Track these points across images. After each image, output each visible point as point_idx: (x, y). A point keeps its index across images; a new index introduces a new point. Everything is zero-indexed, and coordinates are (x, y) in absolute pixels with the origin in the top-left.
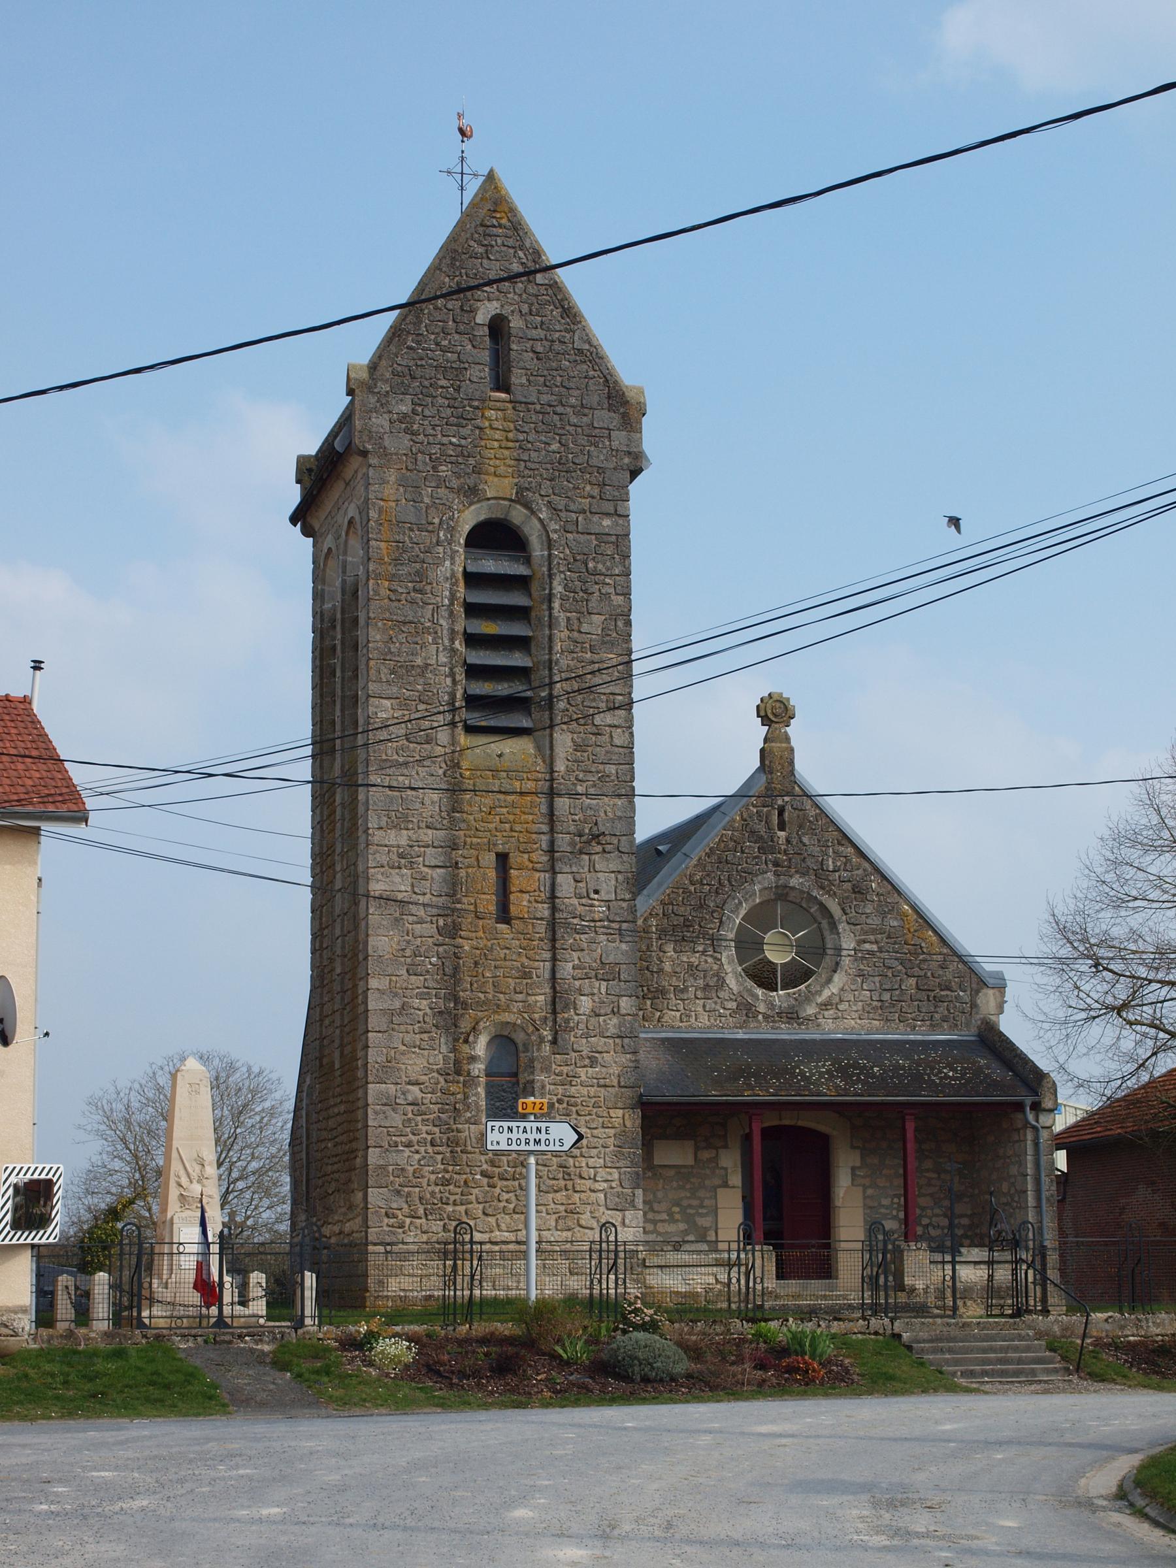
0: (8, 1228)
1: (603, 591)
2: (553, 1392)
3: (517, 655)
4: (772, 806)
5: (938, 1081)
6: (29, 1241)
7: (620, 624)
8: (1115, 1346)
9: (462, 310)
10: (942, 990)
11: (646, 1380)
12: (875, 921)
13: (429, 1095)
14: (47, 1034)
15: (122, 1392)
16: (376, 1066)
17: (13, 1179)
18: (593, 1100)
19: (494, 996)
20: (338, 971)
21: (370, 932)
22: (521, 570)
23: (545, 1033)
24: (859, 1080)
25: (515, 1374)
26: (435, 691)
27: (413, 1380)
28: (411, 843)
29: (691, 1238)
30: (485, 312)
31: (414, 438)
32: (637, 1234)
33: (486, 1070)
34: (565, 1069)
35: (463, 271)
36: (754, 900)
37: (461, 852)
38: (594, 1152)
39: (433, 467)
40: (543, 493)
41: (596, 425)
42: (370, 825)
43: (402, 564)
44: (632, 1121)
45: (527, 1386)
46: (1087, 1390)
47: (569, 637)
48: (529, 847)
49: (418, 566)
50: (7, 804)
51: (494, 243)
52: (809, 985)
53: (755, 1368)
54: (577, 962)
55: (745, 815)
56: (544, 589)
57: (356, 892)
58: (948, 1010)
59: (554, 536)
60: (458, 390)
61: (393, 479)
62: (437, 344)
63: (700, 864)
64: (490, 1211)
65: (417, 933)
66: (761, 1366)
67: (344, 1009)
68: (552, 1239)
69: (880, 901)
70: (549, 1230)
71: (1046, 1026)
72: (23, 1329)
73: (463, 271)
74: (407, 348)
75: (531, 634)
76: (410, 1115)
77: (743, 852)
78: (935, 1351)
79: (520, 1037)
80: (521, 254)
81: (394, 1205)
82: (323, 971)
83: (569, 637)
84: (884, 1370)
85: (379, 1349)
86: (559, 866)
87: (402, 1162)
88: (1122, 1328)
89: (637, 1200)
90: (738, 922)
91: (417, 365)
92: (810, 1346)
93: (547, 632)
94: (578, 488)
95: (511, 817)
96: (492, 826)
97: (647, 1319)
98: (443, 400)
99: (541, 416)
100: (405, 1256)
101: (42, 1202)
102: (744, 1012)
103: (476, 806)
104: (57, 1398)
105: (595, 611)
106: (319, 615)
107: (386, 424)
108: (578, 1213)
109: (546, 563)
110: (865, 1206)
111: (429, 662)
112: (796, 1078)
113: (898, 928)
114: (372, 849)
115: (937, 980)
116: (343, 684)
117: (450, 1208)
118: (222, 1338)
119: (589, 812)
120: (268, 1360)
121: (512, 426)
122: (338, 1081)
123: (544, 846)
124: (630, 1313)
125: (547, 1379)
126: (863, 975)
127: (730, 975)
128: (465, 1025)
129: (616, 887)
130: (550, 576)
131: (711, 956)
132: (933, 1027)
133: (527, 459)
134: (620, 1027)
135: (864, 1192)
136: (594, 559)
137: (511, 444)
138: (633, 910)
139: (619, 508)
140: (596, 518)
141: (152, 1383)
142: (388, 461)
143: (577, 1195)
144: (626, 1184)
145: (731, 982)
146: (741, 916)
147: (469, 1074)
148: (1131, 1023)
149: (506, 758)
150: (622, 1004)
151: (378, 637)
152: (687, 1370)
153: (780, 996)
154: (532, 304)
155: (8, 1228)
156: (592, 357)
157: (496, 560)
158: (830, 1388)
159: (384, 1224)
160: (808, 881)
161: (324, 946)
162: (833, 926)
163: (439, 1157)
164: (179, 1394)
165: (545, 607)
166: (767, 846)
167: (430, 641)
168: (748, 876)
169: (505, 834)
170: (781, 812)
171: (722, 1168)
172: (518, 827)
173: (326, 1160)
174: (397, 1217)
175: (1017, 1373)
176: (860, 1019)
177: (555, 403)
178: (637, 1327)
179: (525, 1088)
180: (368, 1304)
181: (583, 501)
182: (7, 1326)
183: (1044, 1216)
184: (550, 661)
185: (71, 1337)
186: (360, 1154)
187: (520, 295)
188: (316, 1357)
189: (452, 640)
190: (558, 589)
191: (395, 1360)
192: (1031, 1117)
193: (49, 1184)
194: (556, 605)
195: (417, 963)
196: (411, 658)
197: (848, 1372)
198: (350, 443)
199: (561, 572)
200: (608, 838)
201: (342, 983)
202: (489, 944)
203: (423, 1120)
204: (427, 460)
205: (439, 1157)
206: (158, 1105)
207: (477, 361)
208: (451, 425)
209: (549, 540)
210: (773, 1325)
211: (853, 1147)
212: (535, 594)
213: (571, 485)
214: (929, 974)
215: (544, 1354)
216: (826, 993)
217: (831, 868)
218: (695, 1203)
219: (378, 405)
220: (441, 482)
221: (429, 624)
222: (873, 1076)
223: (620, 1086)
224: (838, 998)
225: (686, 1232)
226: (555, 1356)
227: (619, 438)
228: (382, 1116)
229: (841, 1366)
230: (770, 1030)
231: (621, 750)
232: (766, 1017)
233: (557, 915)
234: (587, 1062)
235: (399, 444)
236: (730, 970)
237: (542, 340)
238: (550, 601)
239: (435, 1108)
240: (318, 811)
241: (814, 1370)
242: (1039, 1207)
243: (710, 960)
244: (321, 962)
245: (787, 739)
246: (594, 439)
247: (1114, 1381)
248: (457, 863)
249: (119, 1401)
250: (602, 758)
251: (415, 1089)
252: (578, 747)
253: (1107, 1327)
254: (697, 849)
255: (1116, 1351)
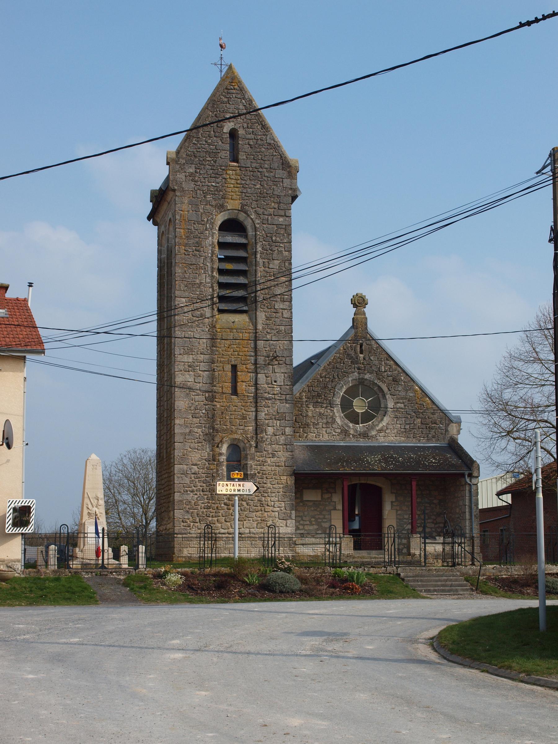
0: (11, 526)
1: (279, 250)
2: (240, 597)
3: (241, 278)
4: (357, 343)
5: (427, 464)
6: (20, 532)
7: (287, 264)
8: (496, 579)
9: (217, 126)
10: (432, 424)
11: (281, 592)
12: (403, 394)
13: (202, 470)
14: (27, 444)
15: (54, 595)
16: (178, 457)
17: (13, 506)
18: (273, 472)
19: (230, 427)
20: (165, 416)
21: (176, 399)
22: (243, 241)
23: (253, 443)
24: (392, 463)
25: (225, 589)
26: (205, 294)
27: (181, 591)
28: (194, 361)
29: (320, 532)
30: (228, 127)
31: (196, 183)
32: (292, 530)
33: (227, 459)
34: (261, 459)
35: (218, 109)
36: (349, 385)
37: (216, 364)
38: (274, 494)
39: (204, 196)
40: (253, 207)
41: (276, 176)
42: (176, 353)
43: (190, 239)
44: (291, 481)
45: (230, 594)
46: (477, 598)
47: (264, 270)
48: (246, 362)
49: (197, 239)
50: (10, 346)
51: (231, 97)
52: (373, 422)
53: (329, 587)
54: (266, 412)
55: (345, 348)
56: (253, 249)
57: (171, 376)
58: (435, 433)
59: (258, 226)
60: (215, 162)
61: (186, 201)
62: (206, 142)
63: (325, 369)
64: (228, 520)
65: (197, 400)
66: (333, 586)
67: (167, 432)
68: (255, 532)
69: (405, 385)
70: (254, 528)
71: (482, 440)
72: (18, 569)
73: (218, 109)
74: (193, 144)
75: (247, 269)
76: (193, 479)
77: (344, 364)
78: (414, 581)
79: (241, 445)
80: (243, 101)
81: (186, 517)
82: (161, 416)
83: (264, 270)
84: (389, 589)
85: (168, 578)
86: (259, 370)
87: (190, 499)
88: (500, 571)
89: (292, 516)
90: (342, 394)
91: (197, 151)
92: (356, 578)
93: (254, 268)
94: (268, 205)
95: (238, 349)
96: (229, 353)
97: (286, 566)
98: (209, 167)
99: (252, 173)
100: (189, 539)
101: (27, 515)
102: (344, 434)
103: (222, 345)
104: (26, 597)
105: (276, 259)
106: (160, 260)
107: (184, 177)
108: (266, 521)
109: (254, 238)
110: (397, 518)
111: (202, 282)
112: (364, 462)
113: (413, 397)
114: (177, 363)
115: (431, 420)
116: (167, 291)
117: (210, 519)
118: (103, 573)
119: (272, 347)
120: (121, 583)
121: (239, 177)
122: (165, 463)
123: (253, 362)
124: (280, 563)
125: (239, 591)
126: (397, 418)
127: (338, 417)
128: (217, 440)
129: (284, 380)
130: (256, 243)
131: (329, 409)
132: (428, 440)
133: (246, 192)
134: (285, 440)
135: (397, 512)
136: (275, 236)
137: (239, 186)
138: (291, 390)
139: (287, 213)
140: (276, 218)
141: (68, 592)
142: (184, 194)
143: (266, 513)
144: (288, 508)
145: (338, 420)
146: (343, 392)
147: (219, 461)
148: (514, 439)
149: (236, 323)
150: (286, 430)
151: (180, 271)
152: (300, 588)
153: (360, 427)
154: (248, 123)
155: (11, 526)
156: (275, 146)
157: (232, 237)
158: (362, 596)
159: (182, 525)
160: (373, 376)
161: (161, 405)
162: (384, 396)
163: (206, 497)
164: (78, 596)
165: (253, 257)
166: (355, 361)
167: (203, 272)
168: (346, 374)
169: (235, 356)
170: (361, 346)
171: (333, 502)
172: (241, 354)
173: (161, 498)
174: (187, 523)
175: (449, 591)
176: (396, 437)
177: (258, 167)
178: (281, 570)
179: (243, 467)
180: (174, 559)
181: (271, 210)
182: (11, 568)
183: (473, 523)
184: (256, 281)
185: (38, 572)
186: (172, 495)
187: (243, 120)
188: (142, 582)
189: (212, 272)
190: (259, 249)
191: (174, 583)
192: (468, 480)
193: (29, 508)
194: (258, 256)
195: (196, 413)
196: (194, 280)
197: (372, 589)
198: (168, 186)
199: (260, 242)
200: (281, 358)
201: (167, 421)
202: (228, 404)
203: (199, 481)
204: (202, 193)
205: (206, 497)
206: (124, 472)
207: (224, 149)
208: (212, 177)
209: (255, 227)
210: (344, 569)
211: (392, 493)
212: (249, 251)
213: (265, 203)
214: (427, 417)
215: (240, 581)
216: (381, 425)
217: (383, 370)
218: (321, 517)
219: (180, 169)
220: (208, 203)
221: (202, 265)
222: (399, 461)
223: (285, 466)
224: (386, 428)
225: (317, 529)
226: (244, 582)
227: (287, 182)
228: (180, 479)
229: (370, 587)
230: (355, 442)
231: (287, 319)
232: (354, 436)
233: (258, 391)
234: (271, 455)
235: (189, 186)
236: (337, 415)
237: (252, 139)
238: (256, 255)
239: (204, 475)
240: (159, 346)
241: (356, 588)
242: (471, 519)
243: (329, 411)
244: (160, 412)
245: (364, 314)
246: (275, 183)
247: (491, 595)
248: (214, 369)
249: (52, 598)
250: (278, 323)
251: (195, 467)
252: (268, 318)
253: (494, 571)
254: (324, 363)
255: (495, 582)
